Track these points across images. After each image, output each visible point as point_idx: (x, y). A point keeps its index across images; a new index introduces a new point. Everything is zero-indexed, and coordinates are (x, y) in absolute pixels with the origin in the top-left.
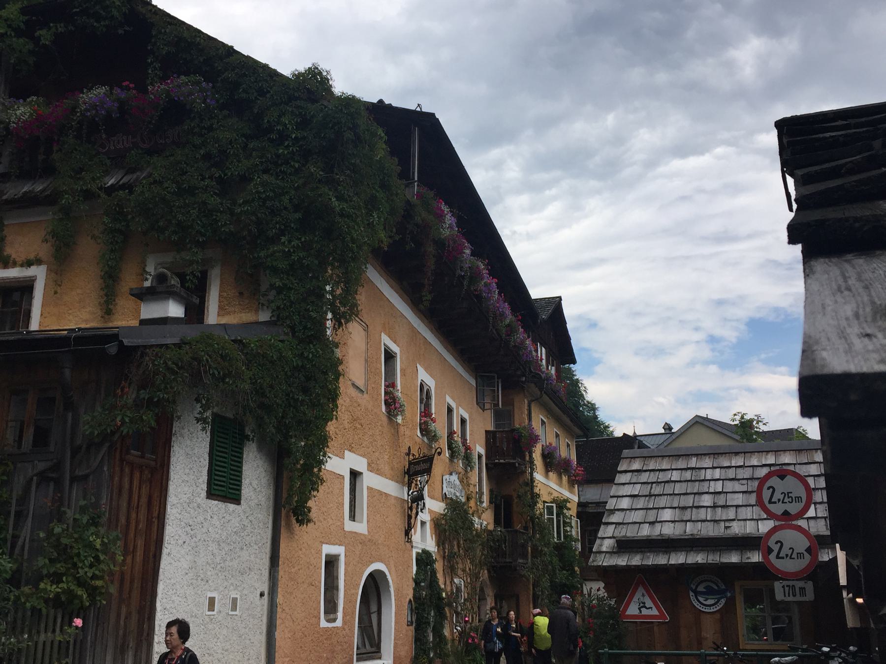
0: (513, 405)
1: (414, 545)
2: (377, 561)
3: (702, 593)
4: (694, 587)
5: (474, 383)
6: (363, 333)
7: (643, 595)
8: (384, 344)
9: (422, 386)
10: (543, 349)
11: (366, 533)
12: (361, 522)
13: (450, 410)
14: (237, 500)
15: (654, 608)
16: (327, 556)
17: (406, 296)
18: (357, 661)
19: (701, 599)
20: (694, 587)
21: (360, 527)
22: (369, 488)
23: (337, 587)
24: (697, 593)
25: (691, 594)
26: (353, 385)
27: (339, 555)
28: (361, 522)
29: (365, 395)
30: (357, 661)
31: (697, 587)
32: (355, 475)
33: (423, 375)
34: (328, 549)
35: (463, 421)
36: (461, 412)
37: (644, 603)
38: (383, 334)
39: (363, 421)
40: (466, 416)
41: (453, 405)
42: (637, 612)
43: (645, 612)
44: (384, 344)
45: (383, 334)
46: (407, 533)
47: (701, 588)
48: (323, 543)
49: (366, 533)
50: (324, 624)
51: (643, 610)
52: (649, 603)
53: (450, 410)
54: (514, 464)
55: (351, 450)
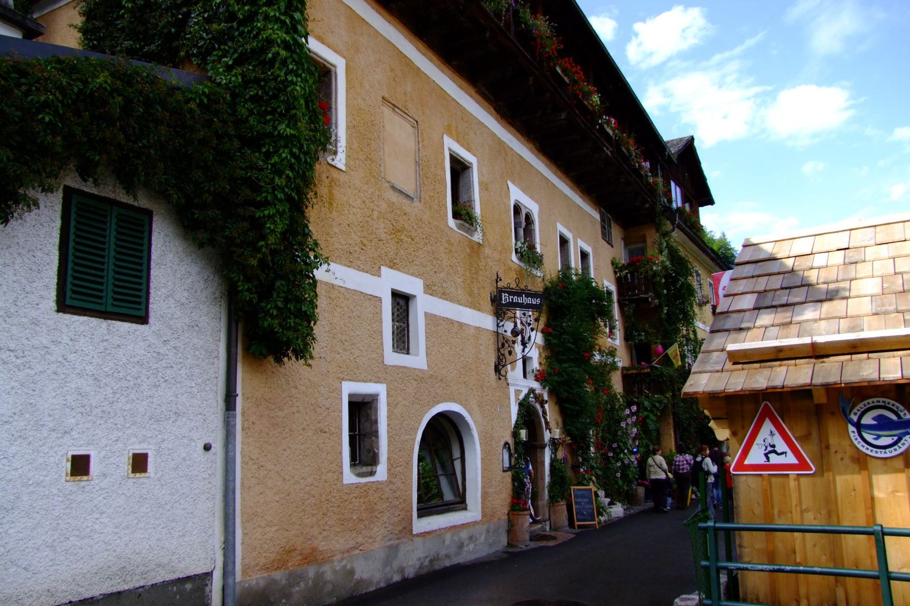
0: (645, 241)
1: (510, 381)
2: (455, 402)
3: (869, 427)
4: (855, 418)
5: (597, 216)
6: (410, 130)
7: (772, 433)
8: (450, 149)
9: (517, 209)
10: (678, 189)
11: (425, 367)
12: (417, 355)
13: (564, 242)
14: (143, 319)
15: (789, 453)
16: (350, 396)
17: (511, 128)
18: (419, 516)
19: (869, 437)
20: (855, 418)
21: (417, 360)
22: (426, 314)
23: (377, 432)
24: (859, 426)
25: (851, 428)
26: (393, 188)
27: (377, 395)
28: (417, 355)
29: (416, 203)
30: (419, 516)
31: (860, 418)
32: (402, 301)
33: (516, 194)
34: (349, 388)
35: (584, 256)
36: (577, 245)
37: (773, 446)
38: (445, 137)
39: (414, 234)
40: (588, 249)
41: (569, 235)
42: (761, 460)
43: (774, 459)
44: (450, 149)
45: (445, 137)
46: (499, 368)
47: (867, 420)
48: (343, 379)
49: (425, 367)
50: (349, 477)
51: (771, 456)
52: (781, 446)
53: (564, 242)
54: (647, 298)
55: (393, 266)
